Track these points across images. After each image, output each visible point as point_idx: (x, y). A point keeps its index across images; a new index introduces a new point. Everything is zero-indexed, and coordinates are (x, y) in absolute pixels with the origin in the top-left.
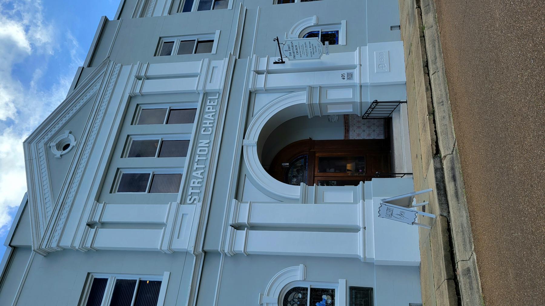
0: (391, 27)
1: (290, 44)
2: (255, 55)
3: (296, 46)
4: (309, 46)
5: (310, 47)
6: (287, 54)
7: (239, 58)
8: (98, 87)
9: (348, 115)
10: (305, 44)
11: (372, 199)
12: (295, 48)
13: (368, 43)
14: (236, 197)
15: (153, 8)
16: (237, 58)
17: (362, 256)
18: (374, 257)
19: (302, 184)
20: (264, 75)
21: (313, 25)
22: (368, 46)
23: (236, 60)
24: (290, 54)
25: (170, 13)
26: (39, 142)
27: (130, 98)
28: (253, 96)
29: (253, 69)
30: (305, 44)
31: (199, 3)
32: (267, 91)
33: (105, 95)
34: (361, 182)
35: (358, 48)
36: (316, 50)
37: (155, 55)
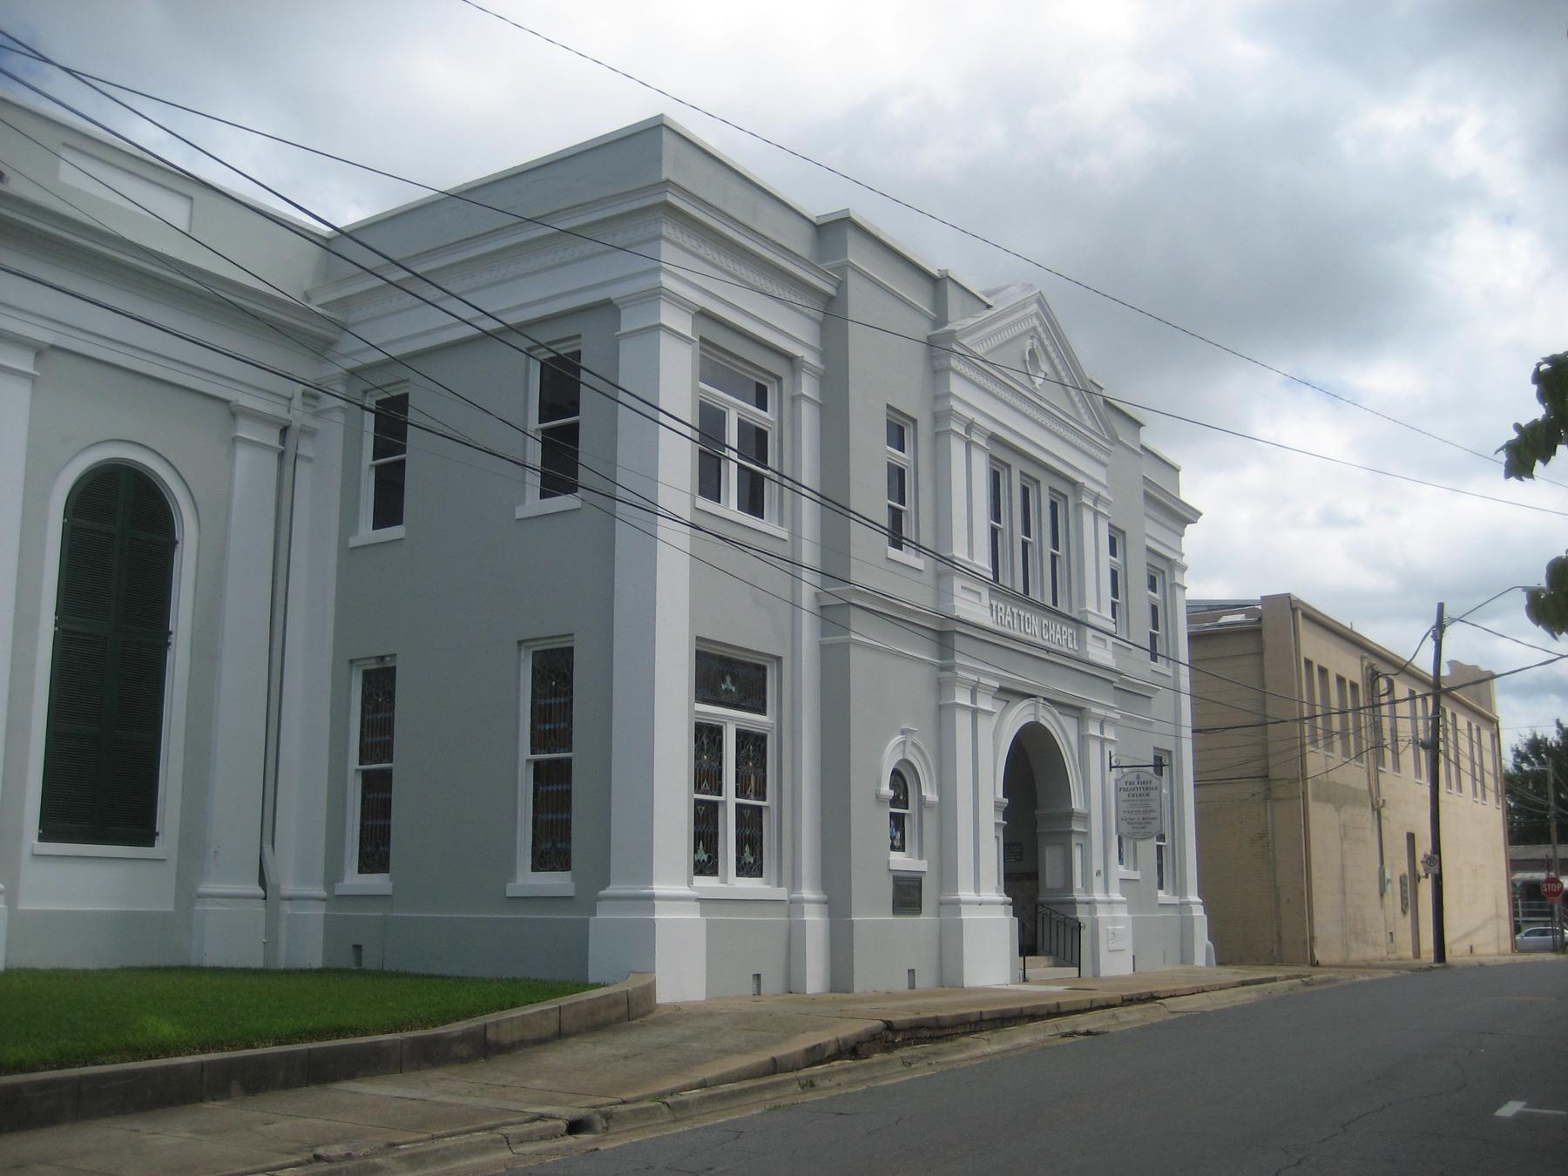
0: (913, 970)
1: (1153, 785)
2: (1118, 717)
3: (1148, 795)
4: (1145, 816)
5: (1143, 819)
6: (1132, 777)
7: (1115, 687)
8: (1089, 424)
9: (1037, 879)
10: (1151, 811)
11: (701, 916)
12: (1142, 792)
13: (1133, 918)
14: (1001, 690)
15: (731, 270)
16: (1115, 685)
17: (608, 891)
18: (597, 917)
19: (1006, 801)
20: (969, 704)
21: (923, 794)
22: (699, 917)
23: (1111, 682)
24: (1130, 784)
25: (1149, 550)
26: (1040, 320)
27: (1073, 483)
28: (1076, 714)
29: (983, 680)
30: (1151, 811)
31: (721, 408)
32: (1083, 739)
33: (1085, 441)
34: (1010, 899)
35: (1124, 899)
36: (1136, 828)
37: (888, 406)
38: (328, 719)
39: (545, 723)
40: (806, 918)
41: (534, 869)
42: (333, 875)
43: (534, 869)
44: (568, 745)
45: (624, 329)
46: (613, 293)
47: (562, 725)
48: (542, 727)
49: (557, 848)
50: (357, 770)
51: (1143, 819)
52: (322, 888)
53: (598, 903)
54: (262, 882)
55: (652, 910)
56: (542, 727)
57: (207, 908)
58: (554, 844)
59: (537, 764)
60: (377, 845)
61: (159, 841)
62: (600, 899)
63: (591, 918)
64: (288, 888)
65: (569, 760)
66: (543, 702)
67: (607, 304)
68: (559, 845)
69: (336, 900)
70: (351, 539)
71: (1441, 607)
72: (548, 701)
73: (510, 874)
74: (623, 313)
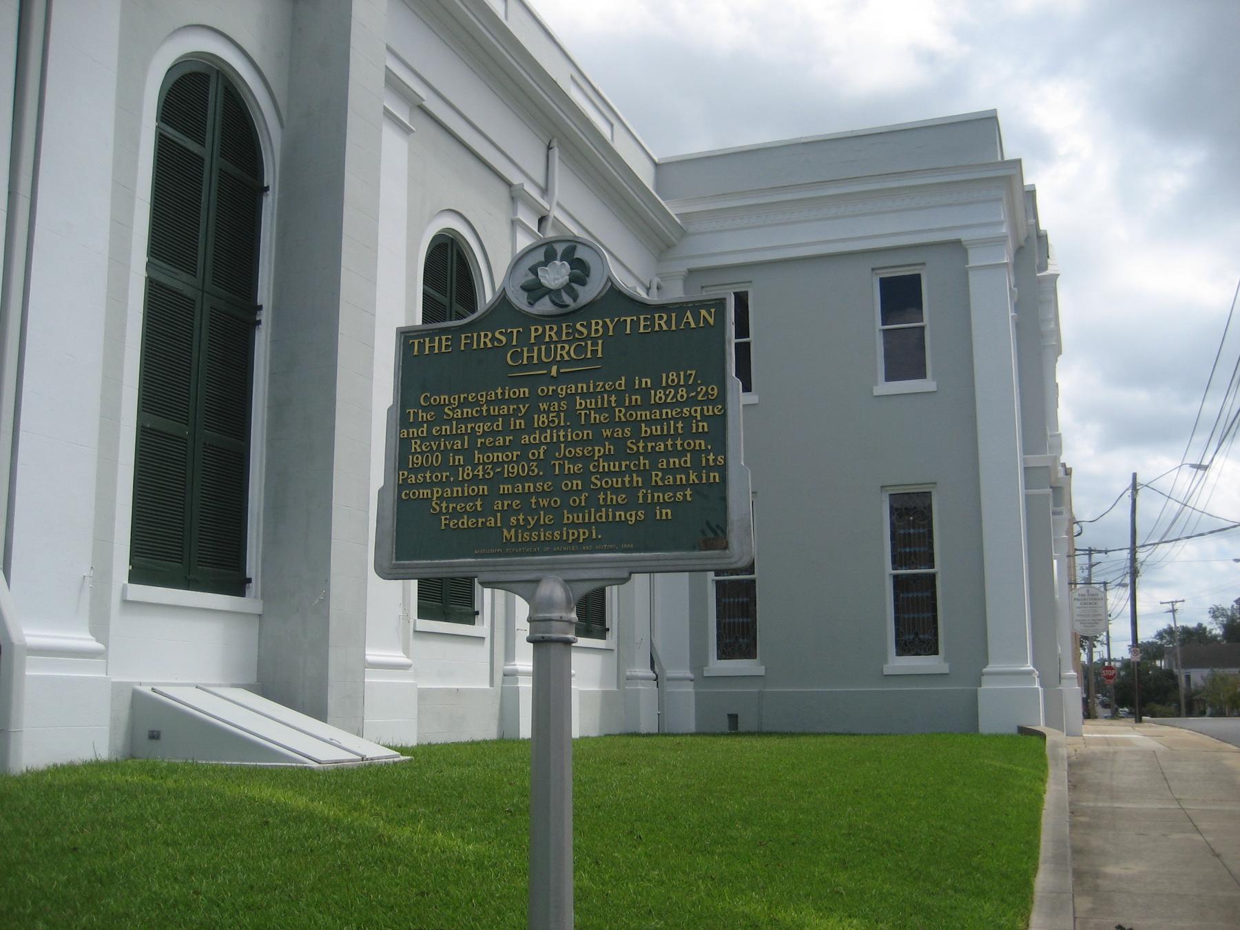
1: (1099, 597)
4: (1095, 618)
12: (1091, 601)
18: (982, 688)
30: (1100, 615)
38: (890, 533)
39: (905, 547)
40: (519, 685)
41: (719, 658)
42: (698, 662)
43: (719, 658)
44: (930, 562)
45: (971, 264)
46: (964, 236)
47: (922, 549)
48: (903, 550)
49: (919, 639)
50: (713, 580)
51: (1093, 620)
52: (688, 671)
53: (982, 677)
54: (652, 667)
55: (517, 681)
56: (903, 550)
57: (639, 688)
58: (917, 634)
59: (896, 577)
60: (737, 638)
61: (608, 635)
62: (983, 675)
63: (979, 688)
64: (670, 673)
65: (753, 581)
66: (902, 532)
67: (957, 243)
68: (922, 636)
69: (701, 679)
70: (875, 388)
71: (1135, 475)
72: (907, 531)
73: (885, 660)
74: (971, 252)
